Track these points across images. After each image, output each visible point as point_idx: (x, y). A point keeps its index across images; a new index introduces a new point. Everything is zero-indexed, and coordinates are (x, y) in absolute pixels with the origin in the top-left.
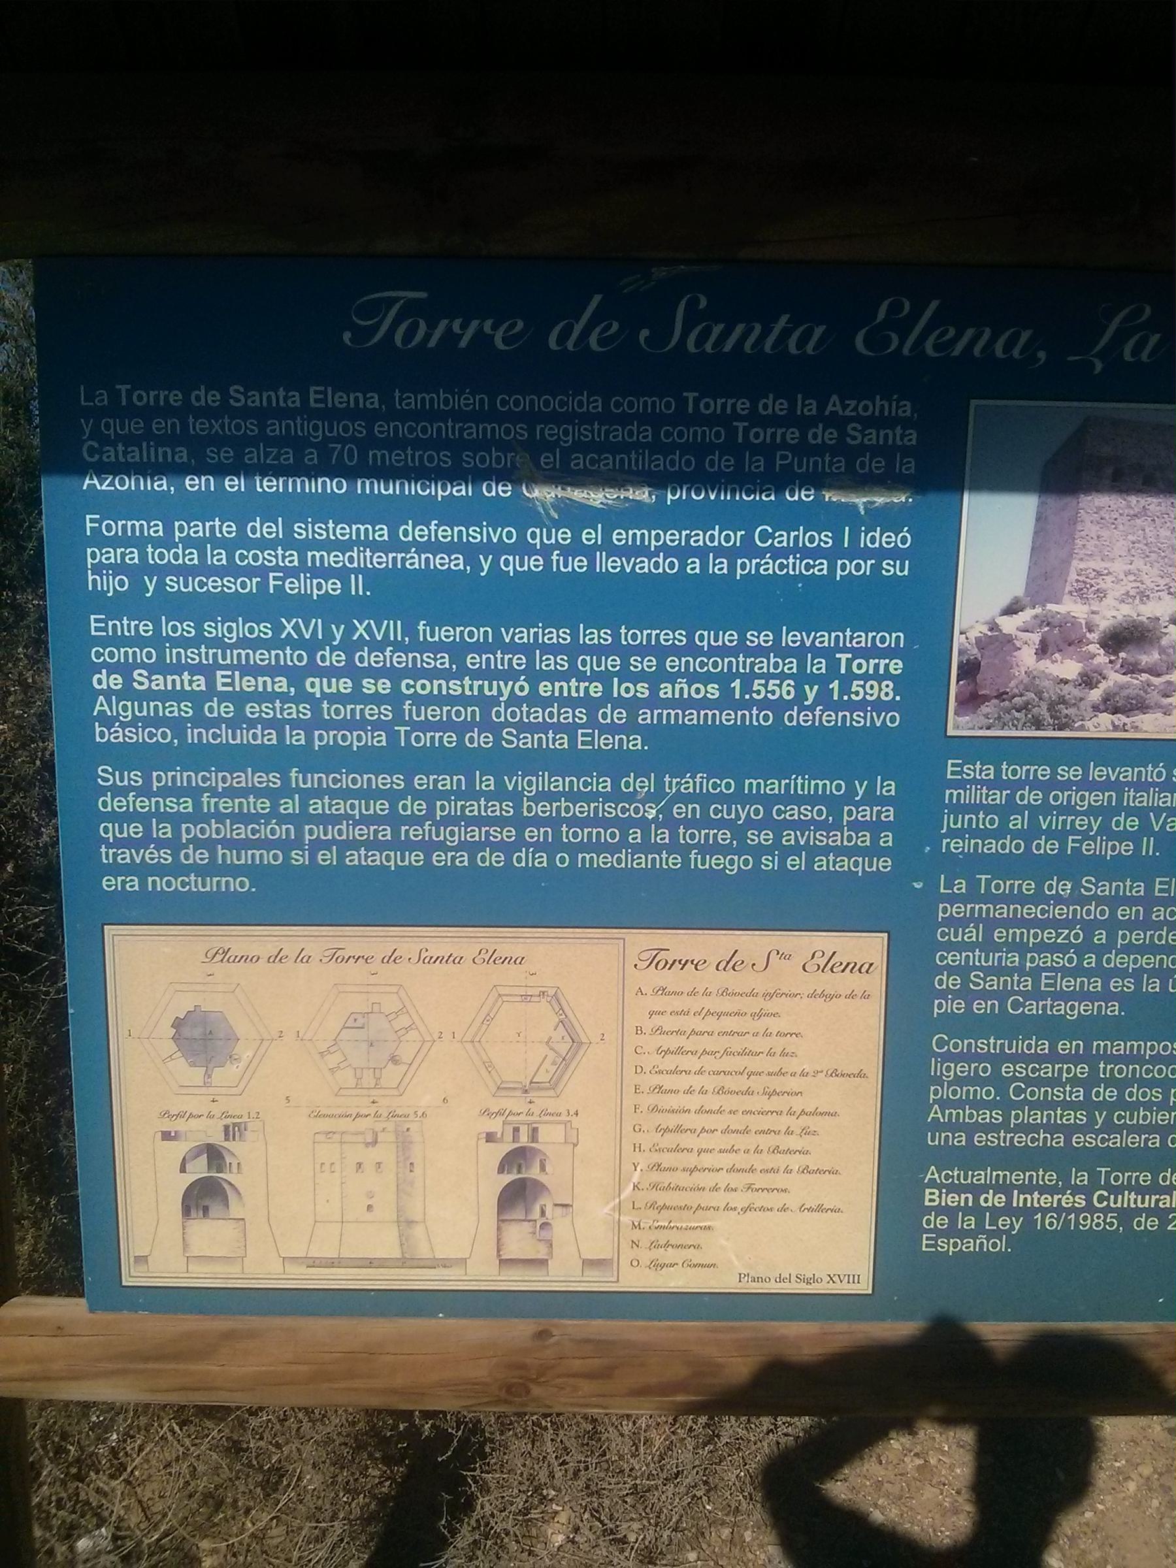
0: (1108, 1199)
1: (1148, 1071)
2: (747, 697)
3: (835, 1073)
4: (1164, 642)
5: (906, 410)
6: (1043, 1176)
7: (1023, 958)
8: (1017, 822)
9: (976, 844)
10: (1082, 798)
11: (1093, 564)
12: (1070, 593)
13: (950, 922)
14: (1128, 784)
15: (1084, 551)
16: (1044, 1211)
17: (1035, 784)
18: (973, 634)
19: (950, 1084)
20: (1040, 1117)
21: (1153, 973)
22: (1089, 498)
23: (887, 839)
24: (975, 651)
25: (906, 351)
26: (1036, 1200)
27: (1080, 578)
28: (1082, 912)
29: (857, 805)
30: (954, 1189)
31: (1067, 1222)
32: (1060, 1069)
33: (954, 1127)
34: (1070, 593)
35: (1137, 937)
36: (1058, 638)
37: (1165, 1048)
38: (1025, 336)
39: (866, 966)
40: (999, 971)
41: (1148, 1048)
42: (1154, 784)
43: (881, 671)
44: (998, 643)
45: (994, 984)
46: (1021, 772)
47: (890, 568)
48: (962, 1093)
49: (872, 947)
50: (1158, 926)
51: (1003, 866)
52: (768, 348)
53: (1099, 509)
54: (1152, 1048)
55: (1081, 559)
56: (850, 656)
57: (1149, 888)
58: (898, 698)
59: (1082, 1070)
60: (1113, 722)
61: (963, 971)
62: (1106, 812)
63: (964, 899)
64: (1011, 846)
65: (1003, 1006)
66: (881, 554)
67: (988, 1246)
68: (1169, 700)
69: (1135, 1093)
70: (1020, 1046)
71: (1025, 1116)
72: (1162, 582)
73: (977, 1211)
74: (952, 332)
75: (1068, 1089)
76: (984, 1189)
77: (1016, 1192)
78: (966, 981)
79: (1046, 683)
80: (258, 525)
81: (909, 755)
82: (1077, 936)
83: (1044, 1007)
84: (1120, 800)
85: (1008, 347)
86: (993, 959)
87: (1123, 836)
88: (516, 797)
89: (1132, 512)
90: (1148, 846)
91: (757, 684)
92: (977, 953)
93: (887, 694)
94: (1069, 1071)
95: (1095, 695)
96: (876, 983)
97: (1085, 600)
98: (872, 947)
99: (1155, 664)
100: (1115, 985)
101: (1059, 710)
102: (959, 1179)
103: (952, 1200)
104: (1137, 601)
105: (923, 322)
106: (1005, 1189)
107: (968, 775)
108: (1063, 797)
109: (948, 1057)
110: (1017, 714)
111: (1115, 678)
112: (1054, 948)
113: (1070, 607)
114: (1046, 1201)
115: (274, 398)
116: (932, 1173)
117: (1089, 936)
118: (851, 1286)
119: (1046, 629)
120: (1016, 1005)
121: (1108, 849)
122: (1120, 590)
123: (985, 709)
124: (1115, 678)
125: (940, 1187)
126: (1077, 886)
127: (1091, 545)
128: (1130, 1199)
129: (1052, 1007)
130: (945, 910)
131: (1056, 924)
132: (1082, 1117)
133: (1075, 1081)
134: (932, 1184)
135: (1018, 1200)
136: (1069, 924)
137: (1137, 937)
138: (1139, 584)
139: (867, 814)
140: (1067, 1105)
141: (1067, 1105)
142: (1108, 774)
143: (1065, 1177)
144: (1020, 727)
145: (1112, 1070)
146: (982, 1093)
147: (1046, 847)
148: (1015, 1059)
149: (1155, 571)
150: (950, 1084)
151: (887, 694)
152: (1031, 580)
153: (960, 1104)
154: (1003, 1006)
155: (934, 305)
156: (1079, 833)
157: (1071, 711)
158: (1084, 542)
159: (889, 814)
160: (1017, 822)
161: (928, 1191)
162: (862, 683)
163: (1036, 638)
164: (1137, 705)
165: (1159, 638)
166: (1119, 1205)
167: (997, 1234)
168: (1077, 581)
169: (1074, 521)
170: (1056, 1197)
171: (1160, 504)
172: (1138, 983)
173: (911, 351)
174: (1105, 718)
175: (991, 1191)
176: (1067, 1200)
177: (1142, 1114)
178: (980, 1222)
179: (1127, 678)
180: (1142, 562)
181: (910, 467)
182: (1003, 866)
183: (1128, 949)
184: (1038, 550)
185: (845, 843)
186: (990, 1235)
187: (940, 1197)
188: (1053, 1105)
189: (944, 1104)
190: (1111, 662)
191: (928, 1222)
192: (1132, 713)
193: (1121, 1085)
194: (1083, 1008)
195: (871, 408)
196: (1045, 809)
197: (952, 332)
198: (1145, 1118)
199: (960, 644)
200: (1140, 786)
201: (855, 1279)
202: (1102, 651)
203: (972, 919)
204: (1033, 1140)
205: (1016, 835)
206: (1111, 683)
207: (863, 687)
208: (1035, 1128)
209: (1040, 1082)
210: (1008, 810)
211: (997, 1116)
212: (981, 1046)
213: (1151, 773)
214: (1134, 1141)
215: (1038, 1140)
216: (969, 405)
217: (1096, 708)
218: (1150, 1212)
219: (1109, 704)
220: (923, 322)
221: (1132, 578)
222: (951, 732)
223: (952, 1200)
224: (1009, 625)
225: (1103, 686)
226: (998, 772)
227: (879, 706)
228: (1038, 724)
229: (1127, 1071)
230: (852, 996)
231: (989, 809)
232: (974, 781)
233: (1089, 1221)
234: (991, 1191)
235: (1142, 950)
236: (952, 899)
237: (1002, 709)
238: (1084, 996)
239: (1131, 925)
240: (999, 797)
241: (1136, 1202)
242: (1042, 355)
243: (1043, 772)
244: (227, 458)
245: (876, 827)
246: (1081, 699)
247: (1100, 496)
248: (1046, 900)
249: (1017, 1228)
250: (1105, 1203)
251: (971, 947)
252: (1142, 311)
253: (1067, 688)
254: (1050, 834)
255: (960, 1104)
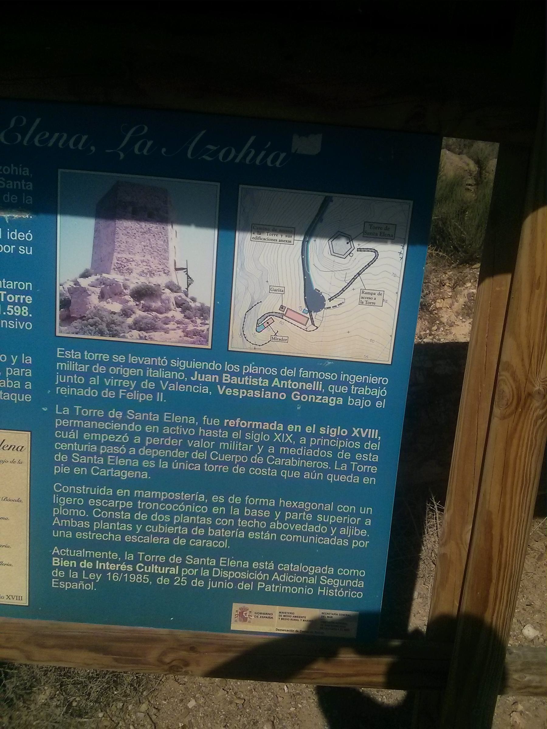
0: (144, 568)
1: (162, 507)
2: (4, 313)
3: (6, 499)
4: (163, 297)
5: (26, 172)
6: (111, 555)
7: (98, 448)
8: (94, 381)
9: (73, 391)
10: (126, 371)
11: (124, 256)
12: (114, 269)
13: (61, 428)
14: (148, 366)
15: (120, 249)
16: (112, 572)
17: (102, 363)
18: (67, 286)
19: (63, 507)
20: (108, 526)
21: (164, 459)
22: (121, 222)
23: (29, 386)
24: (68, 295)
25: (25, 143)
26: (107, 566)
27: (119, 262)
28: (127, 427)
29: (13, 367)
30: (66, 558)
31: (124, 578)
32: (118, 503)
33: (66, 528)
34: (114, 269)
35: (156, 441)
36: (110, 291)
37: (171, 496)
38: (85, 138)
39: (20, 448)
40: (87, 454)
41: (162, 495)
42: (161, 367)
43: (22, 301)
44: (78, 291)
45: (85, 460)
46: (95, 356)
47: (23, 250)
48: (69, 512)
49: (23, 438)
50: (166, 436)
51: (86, 402)
52: (60, 145)
53: (126, 228)
54: (164, 495)
55: (119, 253)
56: (5, 293)
57: (161, 417)
58: (31, 315)
59: (129, 504)
60: (139, 335)
61: (69, 453)
62: (138, 379)
63: (68, 417)
64: (91, 393)
65: (89, 471)
66: (18, 243)
67: (84, 587)
68: (167, 326)
69: (156, 517)
70: (98, 491)
71: (100, 525)
72: (160, 267)
73: (79, 570)
74: (47, 134)
75: (122, 513)
76: (82, 559)
77: (97, 562)
78: (70, 457)
79: (105, 313)
80: (16, 233)
81: (38, 343)
82: (125, 439)
83: (110, 472)
84: (145, 373)
85: (76, 143)
86: (84, 448)
87: (147, 391)
88: (346, 383)
89: (143, 231)
90: (160, 397)
91: (9, 308)
92: (75, 444)
93: (25, 313)
94: (123, 504)
95: (130, 321)
96: (25, 456)
97: (122, 273)
98: (23, 438)
99: (159, 308)
100: (145, 463)
101: (112, 327)
102: (69, 554)
103: (66, 563)
104: (148, 276)
105: (33, 128)
106: (92, 560)
107: (68, 356)
108: (116, 370)
109: (61, 494)
110: (91, 328)
111: (139, 313)
112: (114, 444)
113: (114, 276)
114: (112, 567)
115: (17, 170)
116: (56, 550)
117: (131, 439)
118: (18, 601)
119: (103, 286)
120: (95, 471)
121: (140, 397)
122: (139, 270)
123: (75, 324)
124: (139, 313)
125: (60, 557)
126: (125, 414)
127: (123, 246)
128: (155, 569)
129: (114, 473)
130: (59, 422)
131: (115, 432)
132: (130, 527)
133: (125, 510)
134: (56, 555)
135: (99, 565)
136: (122, 433)
137: (156, 441)
138: (149, 267)
139: (18, 372)
140: (122, 521)
141: (122, 521)
142: (138, 361)
143: (122, 556)
144: (93, 334)
145: (144, 505)
146: (79, 513)
147: (108, 394)
148: (96, 497)
149: (156, 261)
150: (63, 507)
151: (25, 313)
152: (94, 261)
153: (68, 518)
154: (89, 471)
155: (38, 121)
156: (125, 388)
157: (118, 328)
158: (119, 244)
159: (29, 373)
160: (94, 381)
161: (54, 559)
162: (12, 306)
163: (98, 290)
164: (150, 327)
165: (160, 295)
166: (149, 571)
167: (89, 581)
168: (117, 263)
169: (114, 233)
170: (118, 565)
171: (157, 228)
172: (157, 463)
173: (82, 147)
174: (135, 333)
175: (85, 561)
176: (123, 567)
177: (160, 527)
178: (80, 575)
179: (145, 314)
180: (149, 256)
181: (30, 200)
182: (86, 402)
183: (152, 446)
184: (96, 246)
185: (8, 386)
186: (86, 582)
187: (60, 561)
188: (115, 521)
189: (61, 517)
190: (137, 305)
191: (55, 573)
192: (148, 331)
193: (150, 512)
194: (129, 474)
195: (9, 170)
196: (107, 375)
197: (47, 134)
198: (161, 529)
199: (60, 291)
200: (155, 367)
201: (20, 598)
202: (132, 299)
203: (72, 427)
204: (105, 537)
205: (93, 387)
206: (137, 316)
207: (13, 308)
208: (107, 531)
209: (108, 509)
210: (88, 375)
211: (87, 525)
212: (79, 490)
213: (160, 361)
214: (156, 540)
215: (108, 537)
216: (57, 172)
217: (130, 327)
218: (165, 575)
219: (138, 326)
220: (33, 128)
221: (145, 264)
222: (58, 334)
223: (66, 563)
224: (84, 283)
225: (133, 316)
226: (83, 355)
227: (21, 319)
228: (102, 333)
229: (152, 506)
230: (13, 462)
231: (79, 374)
232: (71, 359)
233: (135, 578)
234: (85, 561)
235: (159, 447)
236: (63, 417)
237: (83, 324)
238: (129, 468)
239: (153, 435)
240: (84, 368)
241: (158, 570)
242: (93, 148)
243: (105, 357)
244: (14, 200)
245: (23, 379)
246: (123, 322)
247: (126, 221)
248: (110, 420)
249: (99, 579)
250: (142, 570)
251: (73, 441)
252: (143, 129)
253: (115, 317)
254: (111, 388)
255: (68, 518)
